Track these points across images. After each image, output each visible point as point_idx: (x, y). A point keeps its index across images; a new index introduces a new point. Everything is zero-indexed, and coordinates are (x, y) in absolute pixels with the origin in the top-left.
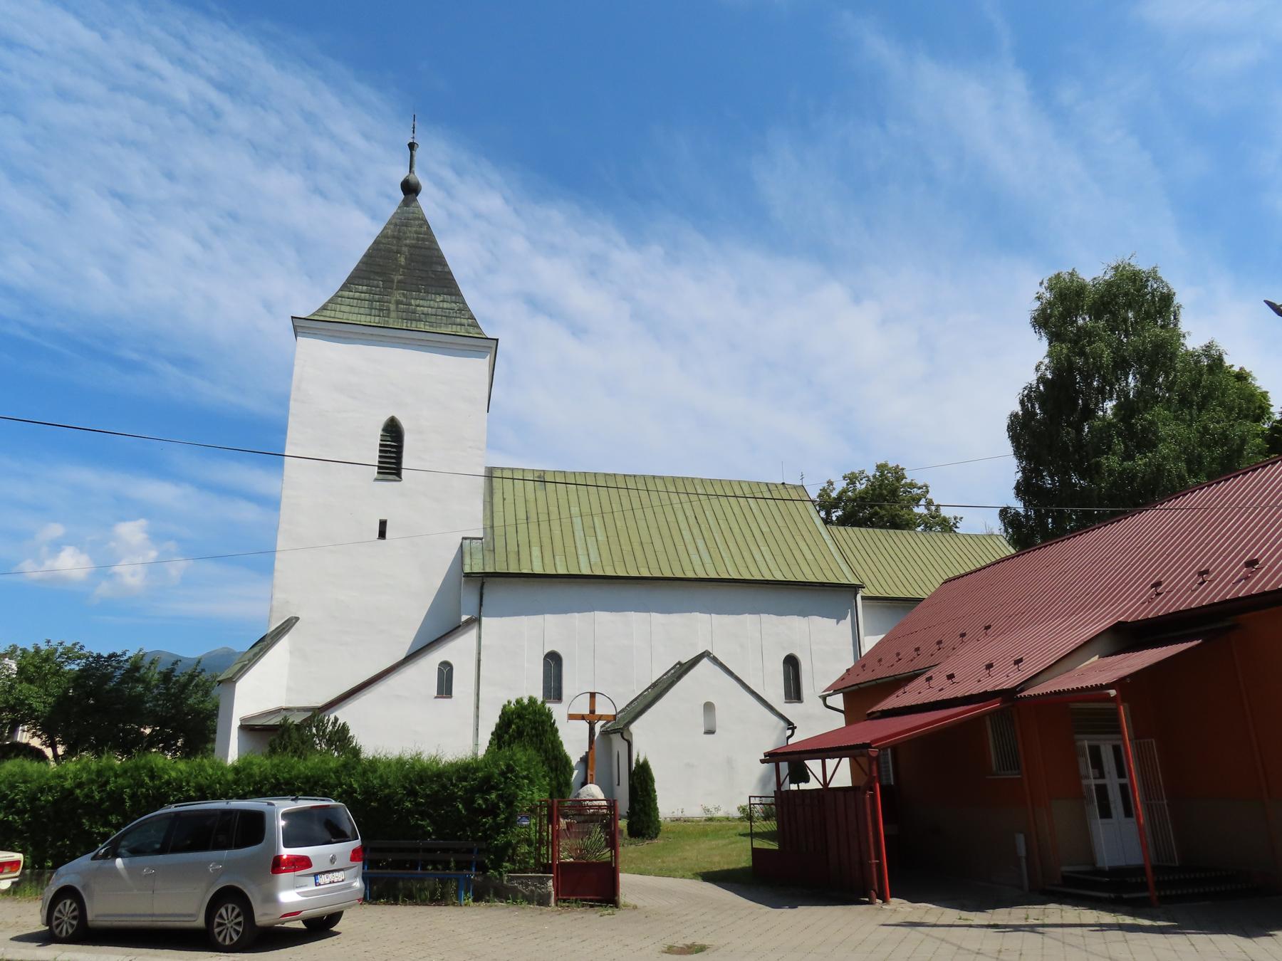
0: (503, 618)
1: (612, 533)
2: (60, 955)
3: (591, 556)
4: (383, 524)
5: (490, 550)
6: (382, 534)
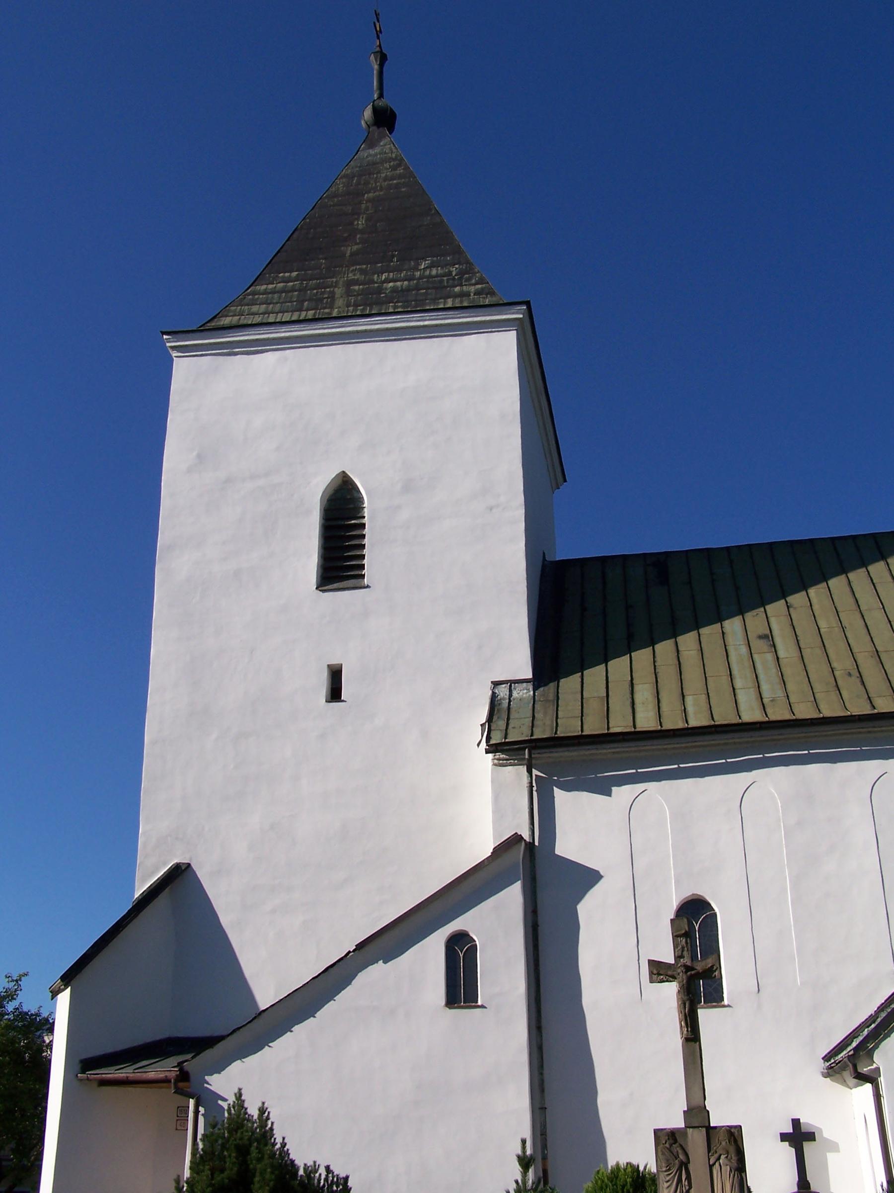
0: (707, 778)
1: (808, 639)
2: (291, 316)
3: (765, 687)
4: (335, 675)
5: (547, 701)
6: (335, 694)
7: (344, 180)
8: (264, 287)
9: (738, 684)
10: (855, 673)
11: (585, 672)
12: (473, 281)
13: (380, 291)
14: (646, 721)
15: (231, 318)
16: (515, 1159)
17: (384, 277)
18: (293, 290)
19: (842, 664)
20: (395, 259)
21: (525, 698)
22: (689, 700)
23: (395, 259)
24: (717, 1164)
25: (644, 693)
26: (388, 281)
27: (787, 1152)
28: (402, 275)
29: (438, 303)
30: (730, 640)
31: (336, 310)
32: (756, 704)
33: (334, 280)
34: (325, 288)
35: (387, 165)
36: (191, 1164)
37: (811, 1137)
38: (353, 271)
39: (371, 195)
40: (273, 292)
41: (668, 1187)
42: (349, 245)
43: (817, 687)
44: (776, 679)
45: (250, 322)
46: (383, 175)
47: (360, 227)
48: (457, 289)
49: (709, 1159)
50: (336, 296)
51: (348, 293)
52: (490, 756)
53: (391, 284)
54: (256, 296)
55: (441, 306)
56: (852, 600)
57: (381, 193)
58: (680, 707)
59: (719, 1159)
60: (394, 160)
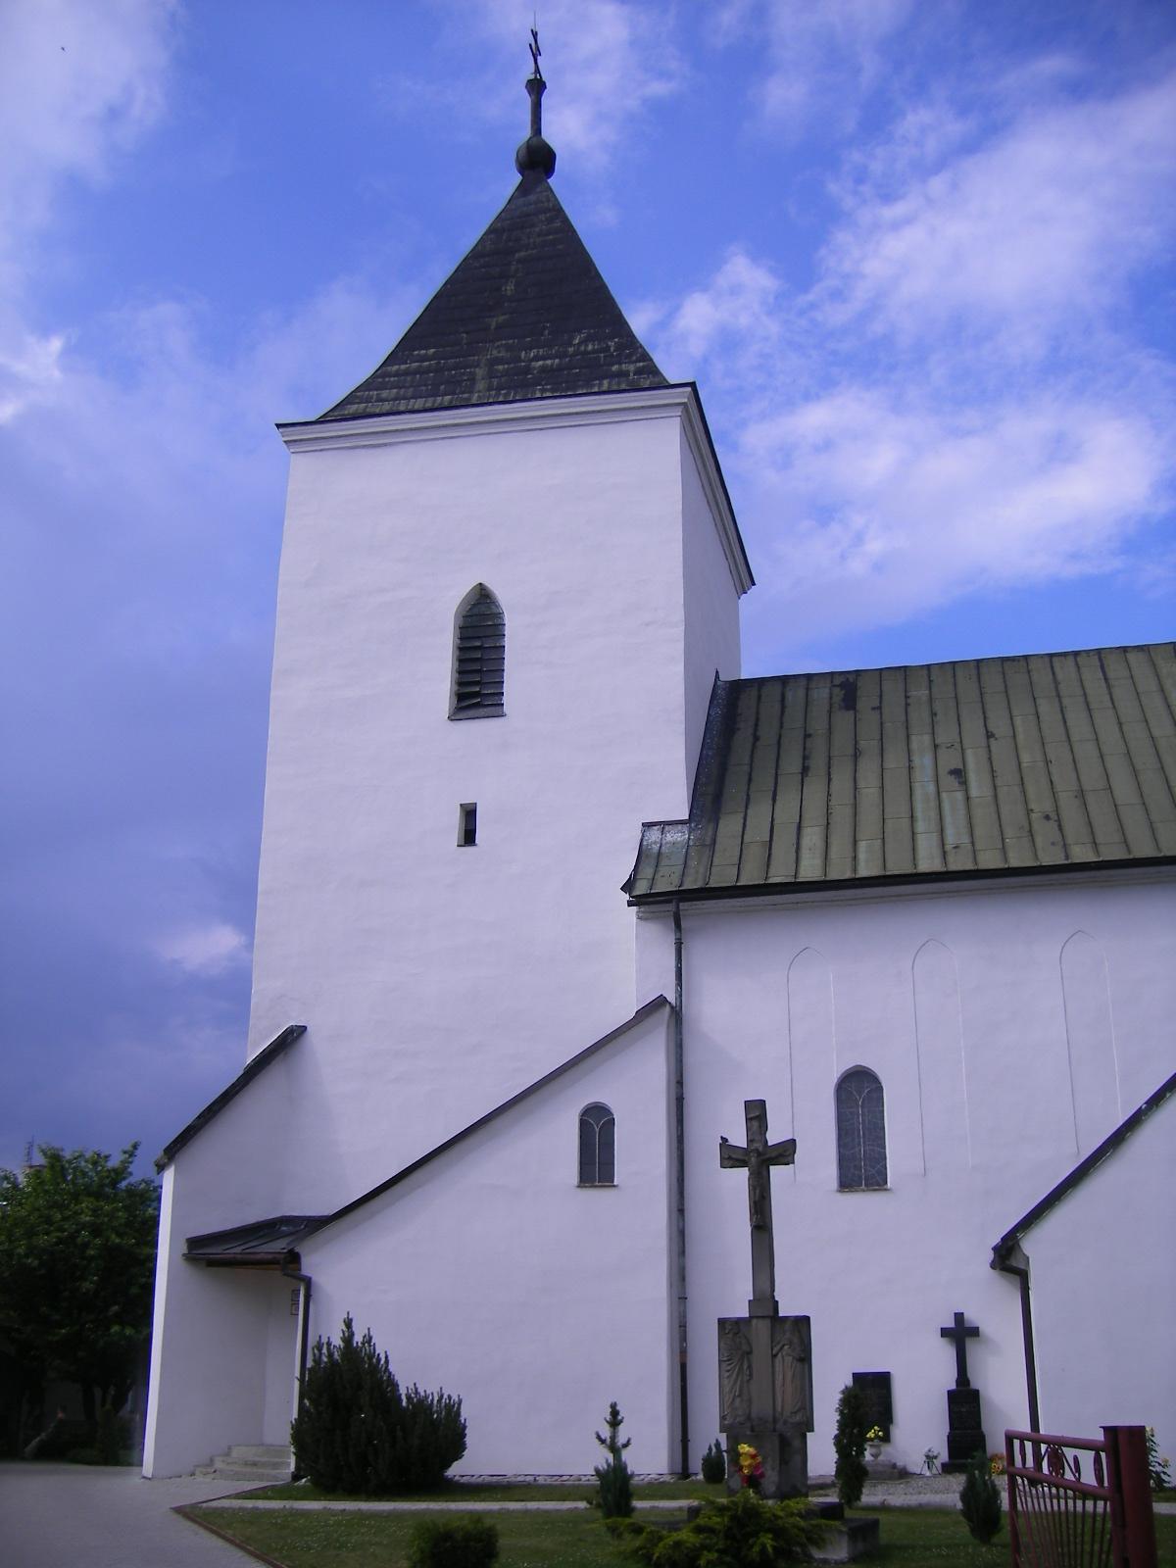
3: (949, 831)
4: (469, 814)
5: (703, 845)
6: (469, 837)
7: (492, 236)
8: (395, 368)
9: (920, 826)
10: (1053, 816)
11: (722, 824)
12: (634, 358)
13: (528, 370)
14: (810, 870)
15: (356, 406)
16: (342, 1320)
17: (532, 354)
18: (428, 371)
19: (1041, 804)
20: (547, 332)
21: (678, 843)
22: (862, 846)
23: (547, 332)
24: (780, 1354)
25: (812, 837)
26: (537, 358)
27: (947, 1353)
28: (554, 351)
29: (594, 386)
30: (917, 775)
31: (476, 395)
32: (937, 852)
33: (476, 358)
34: (465, 368)
35: (542, 217)
36: (982, 1432)
37: (974, 1332)
38: (498, 346)
39: (522, 254)
40: (406, 373)
41: (728, 1377)
42: (494, 316)
43: (1009, 832)
44: (963, 821)
45: (377, 411)
46: (537, 229)
47: (509, 293)
48: (615, 368)
49: (772, 1350)
50: (477, 377)
51: (491, 375)
52: (634, 909)
53: (541, 363)
54: (387, 379)
55: (596, 390)
56: (1062, 730)
57: (534, 251)
58: (850, 854)
59: (781, 1348)
60: (549, 210)
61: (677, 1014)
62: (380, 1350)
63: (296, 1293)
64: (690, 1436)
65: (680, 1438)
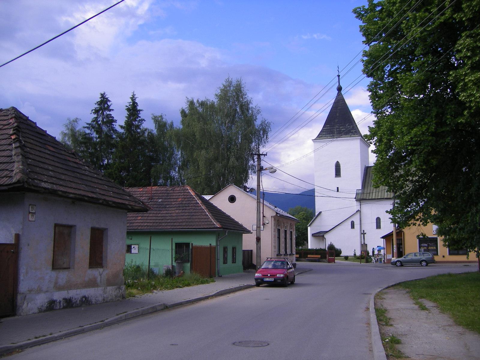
4: (338, 188)
14: (373, 198)
26: (342, 128)
51: (337, 131)
61: (360, 211)
62: (334, 245)
63: (324, 239)
64: (58, 342)
65: (38, 346)
